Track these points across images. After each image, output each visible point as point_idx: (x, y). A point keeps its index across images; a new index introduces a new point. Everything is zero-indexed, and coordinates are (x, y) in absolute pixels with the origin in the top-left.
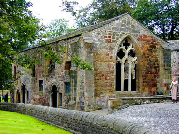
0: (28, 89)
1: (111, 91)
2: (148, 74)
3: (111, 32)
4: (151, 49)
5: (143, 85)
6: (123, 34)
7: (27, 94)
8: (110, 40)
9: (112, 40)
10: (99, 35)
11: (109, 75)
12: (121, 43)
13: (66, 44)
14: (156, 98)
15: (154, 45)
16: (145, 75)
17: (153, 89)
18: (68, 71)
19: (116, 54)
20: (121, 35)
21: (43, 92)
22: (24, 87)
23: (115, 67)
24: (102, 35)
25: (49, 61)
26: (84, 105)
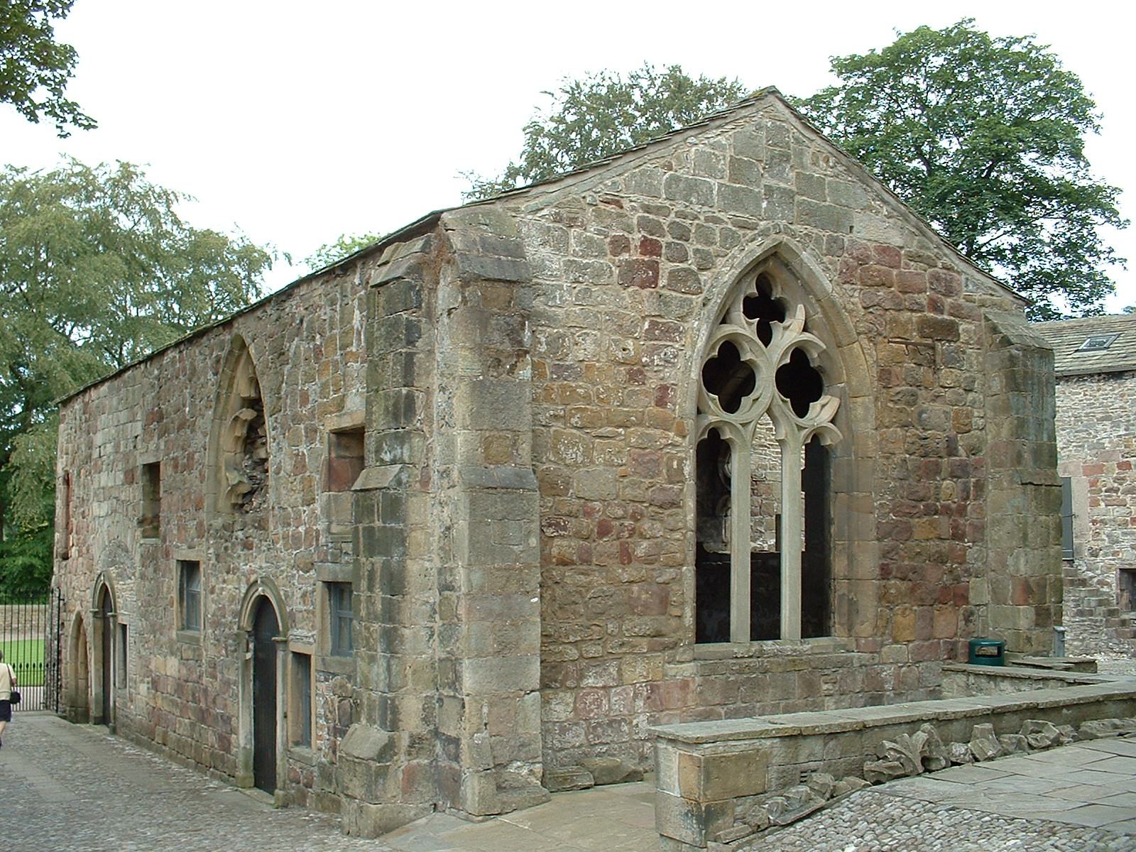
0: (122, 620)
1: (660, 642)
2: (911, 516)
3: (659, 210)
4: (929, 341)
5: (883, 597)
6: (741, 232)
7: (119, 645)
8: (654, 267)
9: (666, 266)
10: (574, 232)
11: (646, 525)
12: (727, 296)
13: (333, 303)
14: (1034, 710)
15: (946, 317)
16: (896, 525)
17: (947, 623)
18: (347, 498)
19: (695, 373)
20: (730, 239)
21: (198, 640)
22: (105, 599)
23: (689, 468)
24: (591, 232)
25: (238, 433)
26: (456, 758)
